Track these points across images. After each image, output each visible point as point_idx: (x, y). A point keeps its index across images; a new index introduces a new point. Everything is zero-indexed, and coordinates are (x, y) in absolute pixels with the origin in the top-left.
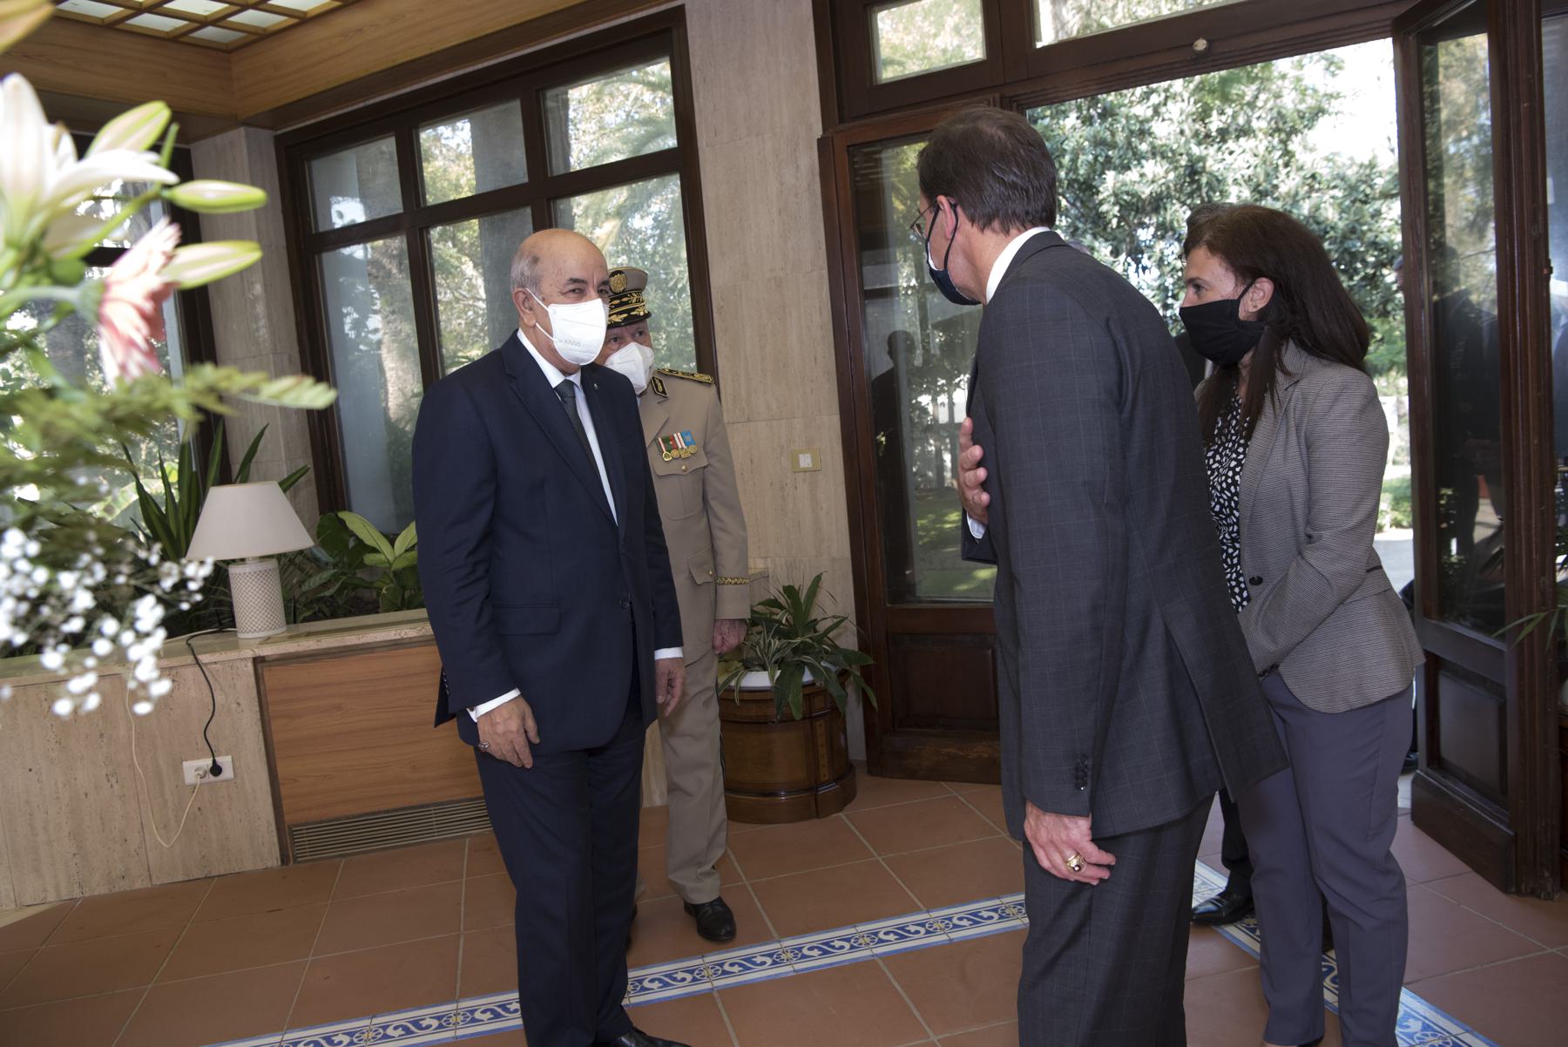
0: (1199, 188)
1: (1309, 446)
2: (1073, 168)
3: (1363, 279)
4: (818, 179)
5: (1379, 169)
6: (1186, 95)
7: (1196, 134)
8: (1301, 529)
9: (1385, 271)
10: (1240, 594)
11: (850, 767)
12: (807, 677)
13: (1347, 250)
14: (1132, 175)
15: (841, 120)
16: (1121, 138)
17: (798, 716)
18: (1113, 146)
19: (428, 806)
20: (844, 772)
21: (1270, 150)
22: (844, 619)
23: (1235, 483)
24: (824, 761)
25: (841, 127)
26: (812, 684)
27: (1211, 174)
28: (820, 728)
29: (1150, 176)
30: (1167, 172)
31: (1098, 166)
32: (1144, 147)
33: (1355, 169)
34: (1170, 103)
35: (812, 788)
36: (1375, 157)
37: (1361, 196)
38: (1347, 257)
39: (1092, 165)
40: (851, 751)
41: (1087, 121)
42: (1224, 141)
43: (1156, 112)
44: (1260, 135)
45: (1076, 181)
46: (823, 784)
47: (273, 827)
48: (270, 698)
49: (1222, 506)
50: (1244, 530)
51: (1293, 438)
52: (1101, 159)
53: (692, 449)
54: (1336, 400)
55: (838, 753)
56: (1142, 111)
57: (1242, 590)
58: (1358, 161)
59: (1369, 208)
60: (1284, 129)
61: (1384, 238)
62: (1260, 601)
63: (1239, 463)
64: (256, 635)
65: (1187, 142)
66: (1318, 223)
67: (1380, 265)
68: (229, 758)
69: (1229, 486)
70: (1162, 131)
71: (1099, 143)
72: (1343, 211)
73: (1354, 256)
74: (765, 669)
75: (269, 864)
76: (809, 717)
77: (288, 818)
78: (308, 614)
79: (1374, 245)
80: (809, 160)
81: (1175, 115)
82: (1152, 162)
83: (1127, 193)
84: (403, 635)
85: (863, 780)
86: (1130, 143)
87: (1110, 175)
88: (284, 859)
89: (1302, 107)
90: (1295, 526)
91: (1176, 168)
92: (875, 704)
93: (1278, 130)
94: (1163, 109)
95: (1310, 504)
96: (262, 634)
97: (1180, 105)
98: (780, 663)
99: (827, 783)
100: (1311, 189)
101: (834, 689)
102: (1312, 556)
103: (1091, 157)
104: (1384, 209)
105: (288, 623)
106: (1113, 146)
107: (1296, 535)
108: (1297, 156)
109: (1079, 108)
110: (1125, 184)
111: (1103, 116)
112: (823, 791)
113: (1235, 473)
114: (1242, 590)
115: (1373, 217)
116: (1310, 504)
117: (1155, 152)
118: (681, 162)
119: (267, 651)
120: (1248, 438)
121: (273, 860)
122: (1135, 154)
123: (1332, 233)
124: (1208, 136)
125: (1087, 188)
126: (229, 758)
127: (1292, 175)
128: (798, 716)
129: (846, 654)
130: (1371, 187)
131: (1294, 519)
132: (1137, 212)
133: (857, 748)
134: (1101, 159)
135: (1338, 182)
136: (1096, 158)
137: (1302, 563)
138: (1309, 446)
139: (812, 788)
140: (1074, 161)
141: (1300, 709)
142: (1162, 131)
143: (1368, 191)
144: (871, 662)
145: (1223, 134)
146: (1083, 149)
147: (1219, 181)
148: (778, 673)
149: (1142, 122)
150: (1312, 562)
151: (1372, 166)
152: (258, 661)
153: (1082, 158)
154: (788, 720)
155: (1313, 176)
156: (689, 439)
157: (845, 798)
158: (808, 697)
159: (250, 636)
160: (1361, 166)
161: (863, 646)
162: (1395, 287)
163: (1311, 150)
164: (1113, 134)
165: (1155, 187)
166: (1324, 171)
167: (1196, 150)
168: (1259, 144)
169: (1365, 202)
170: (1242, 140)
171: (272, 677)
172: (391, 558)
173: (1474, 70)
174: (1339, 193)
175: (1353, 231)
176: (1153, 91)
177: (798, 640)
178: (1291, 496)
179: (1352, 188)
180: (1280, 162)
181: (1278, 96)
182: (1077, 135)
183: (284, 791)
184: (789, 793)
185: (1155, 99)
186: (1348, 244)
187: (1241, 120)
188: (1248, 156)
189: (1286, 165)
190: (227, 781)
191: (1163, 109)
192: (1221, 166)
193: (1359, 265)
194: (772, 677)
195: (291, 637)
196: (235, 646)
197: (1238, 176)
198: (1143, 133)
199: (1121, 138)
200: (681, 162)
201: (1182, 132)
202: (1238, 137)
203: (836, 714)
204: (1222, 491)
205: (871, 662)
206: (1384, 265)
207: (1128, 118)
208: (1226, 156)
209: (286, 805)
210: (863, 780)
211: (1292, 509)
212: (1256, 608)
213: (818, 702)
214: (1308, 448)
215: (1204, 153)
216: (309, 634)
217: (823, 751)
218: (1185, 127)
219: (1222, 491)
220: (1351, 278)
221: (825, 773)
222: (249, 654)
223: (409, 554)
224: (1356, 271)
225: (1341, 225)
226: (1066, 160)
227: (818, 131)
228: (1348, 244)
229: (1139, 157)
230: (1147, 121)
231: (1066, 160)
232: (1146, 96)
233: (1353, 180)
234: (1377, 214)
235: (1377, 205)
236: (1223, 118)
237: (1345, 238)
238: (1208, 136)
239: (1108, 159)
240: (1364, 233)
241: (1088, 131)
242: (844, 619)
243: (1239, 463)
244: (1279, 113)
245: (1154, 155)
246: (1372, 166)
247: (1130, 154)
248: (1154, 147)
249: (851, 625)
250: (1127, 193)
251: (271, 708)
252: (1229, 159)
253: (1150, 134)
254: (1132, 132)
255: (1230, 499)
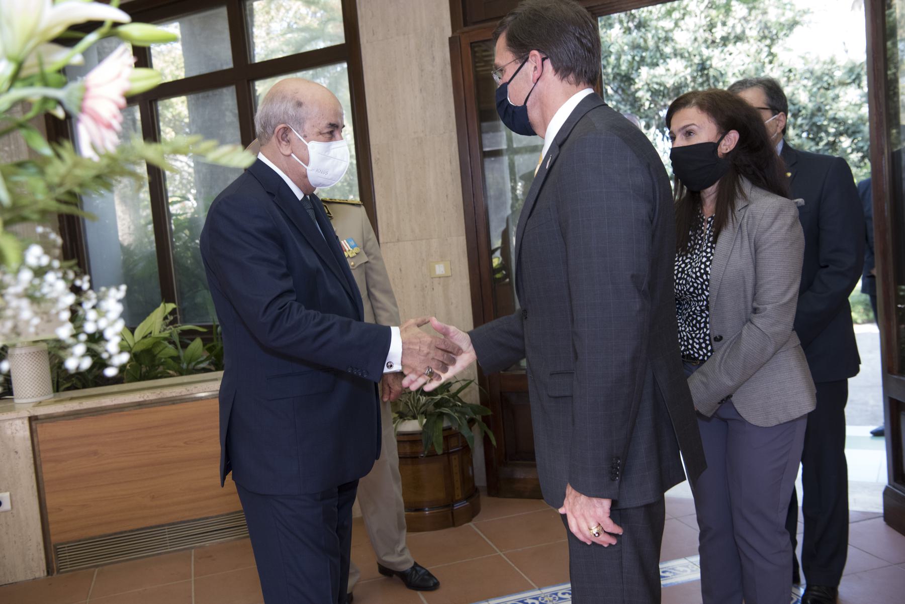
0: (708, 80)
1: (756, 250)
2: (618, 66)
3: (827, 144)
4: (449, 67)
5: (838, 64)
6: (698, 13)
7: (706, 41)
8: (749, 304)
9: (843, 139)
10: (706, 348)
11: (476, 490)
12: (446, 423)
13: (814, 124)
14: (660, 70)
15: (465, 25)
16: (651, 43)
17: (440, 451)
18: (646, 49)
19: (163, 526)
20: (472, 493)
21: (759, 52)
22: (471, 382)
23: (706, 273)
24: (458, 484)
25: (466, 29)
26: (450, 428)
27: (716, 69)
28: (455, 461)
29: (673, 71)
30: (686, 67)
31: (635, 64)
32: (668, 50)
33: (820, 65)
34: (687, 18)
35: (449, 504)
36: (834, 56)
37: (825, 85)
38: (815, 129)
39: (631, 63)
40: (476, 479)
41: (628, 31)
42: (725, 45)
43: (676, 25)
44: (752, 41)
45: (619, 74)
46: (457, 502)
47: (42, 546)
48: (42, 447)
49: (696, 288)
50: (712, 305)
51: (746, 243)
52: (637, 59)
53: (357, 250)
54: (776, 218)
55: (467, 479)
56: (668, 24)
57: (707, 345)
58: (822, 59)
59: (831, 93)
60: (769, 36)
61: (841, 115)
62: (721, 352)
63: (708, 258)
64: (30, 400)
65: (699, 46)
66: (794, 104)
67: (839, 134)
68: (8, 494)
69: (702, 275)
70: (682, 39)
71: (635, 47)
72: (812, 96)
73: (820, 128)
74: (414, 418)
75: (37, 575)
76: (447, 453)
77: (54, 539)
78: (68, 385)
79: (834, 119)
80: (443, 53)
81: (692, 27)
82: (674, 60)
83: (657, 83)
84: (146, 398)
85: (485, 500)
86: (658, 47)
87: (644, 70)
88: (49, 571)
89: (782, 20)
90: (746, 302)
91: (691, 66)
92: (494, 443)
93: (765, 37)
94: (681, 23)
95: (756, 286)
96: (34, 400)
97: (694, 19)
98: (425, 413)
99: (459, 501)
100: (789, 78)
101: (465, 431)
102: (758, 321)
103: (630, 58)
104: (841, 94)
105: (54, 392)
106: (646, 49)
107: (746, 308)
108: (779, 56)
109: (621, 22)
110: (655, 76)
111: (639, 26)
112: (457, 506)
113: (706, 266)
114: (707, 345)
115: (833, 99)
116: (756, 286)
117: (676, 54)
118: (348, 52)
119: (41, 411)
120: (715, 241)
121: (40, 571)
122: (661, 55)
123: (804, 112)
124: (713, 42)
125: (627, 79)
126: (8, 494)
127: (774, 70)
128: (440, 451)
129: (472, 407)
130: (832, 77)
131: (745, 297)
132: (664, 96)
133: (480, 479)
134: (637, 59)
135: (808, 75)
136: (633, 58)
137: (752, 326)
138: (756, 250)
139: (449, 504)
140: (618, 59)
141: (743, 421)
142: (682, 39)
143: (830, 81)
144: (490, 413)
145: (725, 40)
146: (623, 51)
147: (722, 75)
148: (425, 421)
149: (666, 32)
150: (759, 325)
151: (832, 62)
152: (32, 419)
153: (623, 58)
154: (432, 455)
155: (790, 71)
156: (352, 243)
157: (473, 513)
158: (446, 438)
159: (24, 401)
160: (824, 63)
161: (484, 401)
162: (849, 150)
163: (789, 50)
164: (645, 41)
165: (677, 79)
166: (800, 66)
167: (706, 53)
168: (751, 46)
169: (827, 89)
170: (738, 44)
171: (44, 431)
172: (132, 344)
173: (708, 47)
174: (810, 83)
175: (819, 109)
176: (674, 9)
177: (439, 397)
178: (744, 282)
179: (819, 79)
180: (767, 60)
181: (765, 13)
182: (620, 41)
183: (51, 518)
184: (431, 508)
185: (676, 15)
186: (815, 119)
187: (738, 30)
188: (743, 56)
189: (771, 62)
190: (6, 512)
191: (681, 23)
192: (724, 63)
193: (823, 134)
194: (421, 423)
195: (56, 402)
196: (12, 409)
197: (736, 71)
198: (667, 39)
199: (651, 43)
200: (348, 52)
201: (696, 39)
202: (735, 43)
203: (466, 449)
204: (697, 277)
205: (490, 413)
206: (841, 134)
207: (656, 29)
208: (727, 56)
209: (52, 528)
210: (485, 500)
211: (745, 291)
212: (719, 357)
213: (453, 442)
214: (756, 251)
215: (711, 54)
216: (72, 399)
217: (457, 478)
218: (698, 35)
219: (697, 277)
220: (817, 144)
221: (458, 494)
222: (27, 414)
223: (146, 340)
224: (821, 139)
225: (810, 106)
226: (612, 59)
227: (448, 33)
228: (815, 119)
229: (664, 57)
230: (671, 31)
231: (612, 59)
232: (669, 13)
233: (819, 73)
234: (836, 98)
235: (837, 91)
236: (726, 28)
237: (813, 115)
238: (713, 42)
239: (643, 59)
240: (827, 111)
241: (628, 39)
242: (471, 382)
243: (708, 258)
244: (766, 24)
245: (676, 55)
246: (832, 62)
247: (658, 55)
248: (675, 50)
249: (475, 387)
250: (657, 83)
251: (42, 455)
252: (729, 58)
253: (673, 40)
254: (659, 39)
255: (702, 284)
